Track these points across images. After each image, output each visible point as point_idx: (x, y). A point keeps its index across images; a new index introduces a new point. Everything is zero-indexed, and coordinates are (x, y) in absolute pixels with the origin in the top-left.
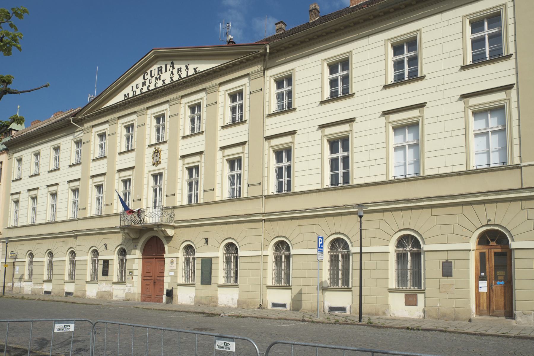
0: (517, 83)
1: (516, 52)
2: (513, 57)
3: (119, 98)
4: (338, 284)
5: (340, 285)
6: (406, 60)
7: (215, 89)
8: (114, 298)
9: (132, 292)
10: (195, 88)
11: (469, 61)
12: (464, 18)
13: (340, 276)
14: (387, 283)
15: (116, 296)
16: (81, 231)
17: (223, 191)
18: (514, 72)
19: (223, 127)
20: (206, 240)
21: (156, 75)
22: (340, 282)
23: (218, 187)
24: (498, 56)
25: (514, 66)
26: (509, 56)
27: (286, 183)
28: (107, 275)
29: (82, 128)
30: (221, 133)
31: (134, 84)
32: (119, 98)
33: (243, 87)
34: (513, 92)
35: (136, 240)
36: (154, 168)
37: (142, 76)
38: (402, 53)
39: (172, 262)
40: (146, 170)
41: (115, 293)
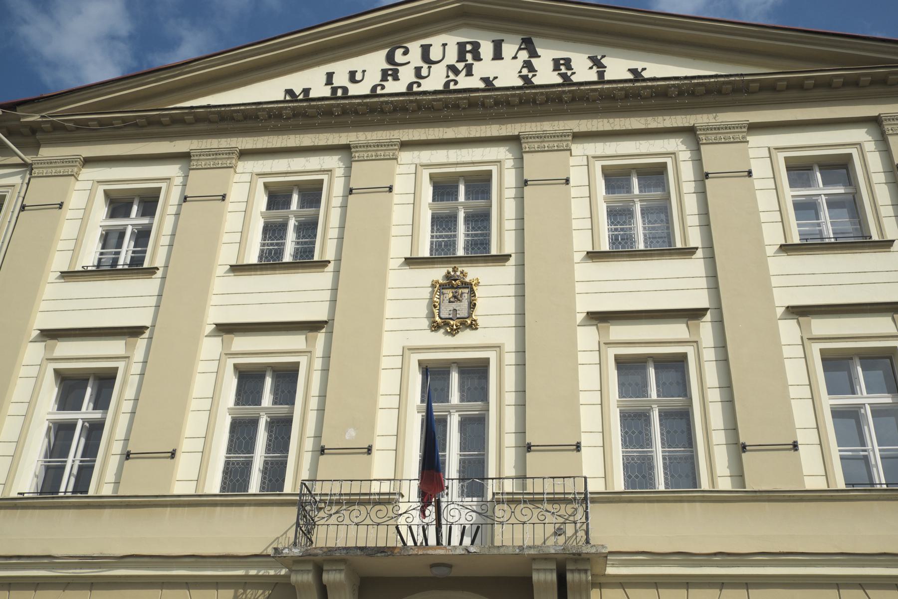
0: (153, 326)
1: (166, 267)
2: (331, 267)
3: (268, 91)
6: (292, 223)
7: (68, 169)
10: (336, 135)
11: (425, 252)
12: (419, 168)
16: (47, 560)
17: (199, 467)
18: (153, 301)
19: (68, 275)
21: (452, 57)
23: (188, 446)
24: (305, 260)
26: (324, 264)
27: (75, 471)
29: (28, 159)
30: (53, 290)
31: (355, 63)
32: (268, 91)
33: (164, 185)
34: (141, 343)
36: (440, 338)
37: (383, 53)
38: (127, 215)
40: (391, 345)
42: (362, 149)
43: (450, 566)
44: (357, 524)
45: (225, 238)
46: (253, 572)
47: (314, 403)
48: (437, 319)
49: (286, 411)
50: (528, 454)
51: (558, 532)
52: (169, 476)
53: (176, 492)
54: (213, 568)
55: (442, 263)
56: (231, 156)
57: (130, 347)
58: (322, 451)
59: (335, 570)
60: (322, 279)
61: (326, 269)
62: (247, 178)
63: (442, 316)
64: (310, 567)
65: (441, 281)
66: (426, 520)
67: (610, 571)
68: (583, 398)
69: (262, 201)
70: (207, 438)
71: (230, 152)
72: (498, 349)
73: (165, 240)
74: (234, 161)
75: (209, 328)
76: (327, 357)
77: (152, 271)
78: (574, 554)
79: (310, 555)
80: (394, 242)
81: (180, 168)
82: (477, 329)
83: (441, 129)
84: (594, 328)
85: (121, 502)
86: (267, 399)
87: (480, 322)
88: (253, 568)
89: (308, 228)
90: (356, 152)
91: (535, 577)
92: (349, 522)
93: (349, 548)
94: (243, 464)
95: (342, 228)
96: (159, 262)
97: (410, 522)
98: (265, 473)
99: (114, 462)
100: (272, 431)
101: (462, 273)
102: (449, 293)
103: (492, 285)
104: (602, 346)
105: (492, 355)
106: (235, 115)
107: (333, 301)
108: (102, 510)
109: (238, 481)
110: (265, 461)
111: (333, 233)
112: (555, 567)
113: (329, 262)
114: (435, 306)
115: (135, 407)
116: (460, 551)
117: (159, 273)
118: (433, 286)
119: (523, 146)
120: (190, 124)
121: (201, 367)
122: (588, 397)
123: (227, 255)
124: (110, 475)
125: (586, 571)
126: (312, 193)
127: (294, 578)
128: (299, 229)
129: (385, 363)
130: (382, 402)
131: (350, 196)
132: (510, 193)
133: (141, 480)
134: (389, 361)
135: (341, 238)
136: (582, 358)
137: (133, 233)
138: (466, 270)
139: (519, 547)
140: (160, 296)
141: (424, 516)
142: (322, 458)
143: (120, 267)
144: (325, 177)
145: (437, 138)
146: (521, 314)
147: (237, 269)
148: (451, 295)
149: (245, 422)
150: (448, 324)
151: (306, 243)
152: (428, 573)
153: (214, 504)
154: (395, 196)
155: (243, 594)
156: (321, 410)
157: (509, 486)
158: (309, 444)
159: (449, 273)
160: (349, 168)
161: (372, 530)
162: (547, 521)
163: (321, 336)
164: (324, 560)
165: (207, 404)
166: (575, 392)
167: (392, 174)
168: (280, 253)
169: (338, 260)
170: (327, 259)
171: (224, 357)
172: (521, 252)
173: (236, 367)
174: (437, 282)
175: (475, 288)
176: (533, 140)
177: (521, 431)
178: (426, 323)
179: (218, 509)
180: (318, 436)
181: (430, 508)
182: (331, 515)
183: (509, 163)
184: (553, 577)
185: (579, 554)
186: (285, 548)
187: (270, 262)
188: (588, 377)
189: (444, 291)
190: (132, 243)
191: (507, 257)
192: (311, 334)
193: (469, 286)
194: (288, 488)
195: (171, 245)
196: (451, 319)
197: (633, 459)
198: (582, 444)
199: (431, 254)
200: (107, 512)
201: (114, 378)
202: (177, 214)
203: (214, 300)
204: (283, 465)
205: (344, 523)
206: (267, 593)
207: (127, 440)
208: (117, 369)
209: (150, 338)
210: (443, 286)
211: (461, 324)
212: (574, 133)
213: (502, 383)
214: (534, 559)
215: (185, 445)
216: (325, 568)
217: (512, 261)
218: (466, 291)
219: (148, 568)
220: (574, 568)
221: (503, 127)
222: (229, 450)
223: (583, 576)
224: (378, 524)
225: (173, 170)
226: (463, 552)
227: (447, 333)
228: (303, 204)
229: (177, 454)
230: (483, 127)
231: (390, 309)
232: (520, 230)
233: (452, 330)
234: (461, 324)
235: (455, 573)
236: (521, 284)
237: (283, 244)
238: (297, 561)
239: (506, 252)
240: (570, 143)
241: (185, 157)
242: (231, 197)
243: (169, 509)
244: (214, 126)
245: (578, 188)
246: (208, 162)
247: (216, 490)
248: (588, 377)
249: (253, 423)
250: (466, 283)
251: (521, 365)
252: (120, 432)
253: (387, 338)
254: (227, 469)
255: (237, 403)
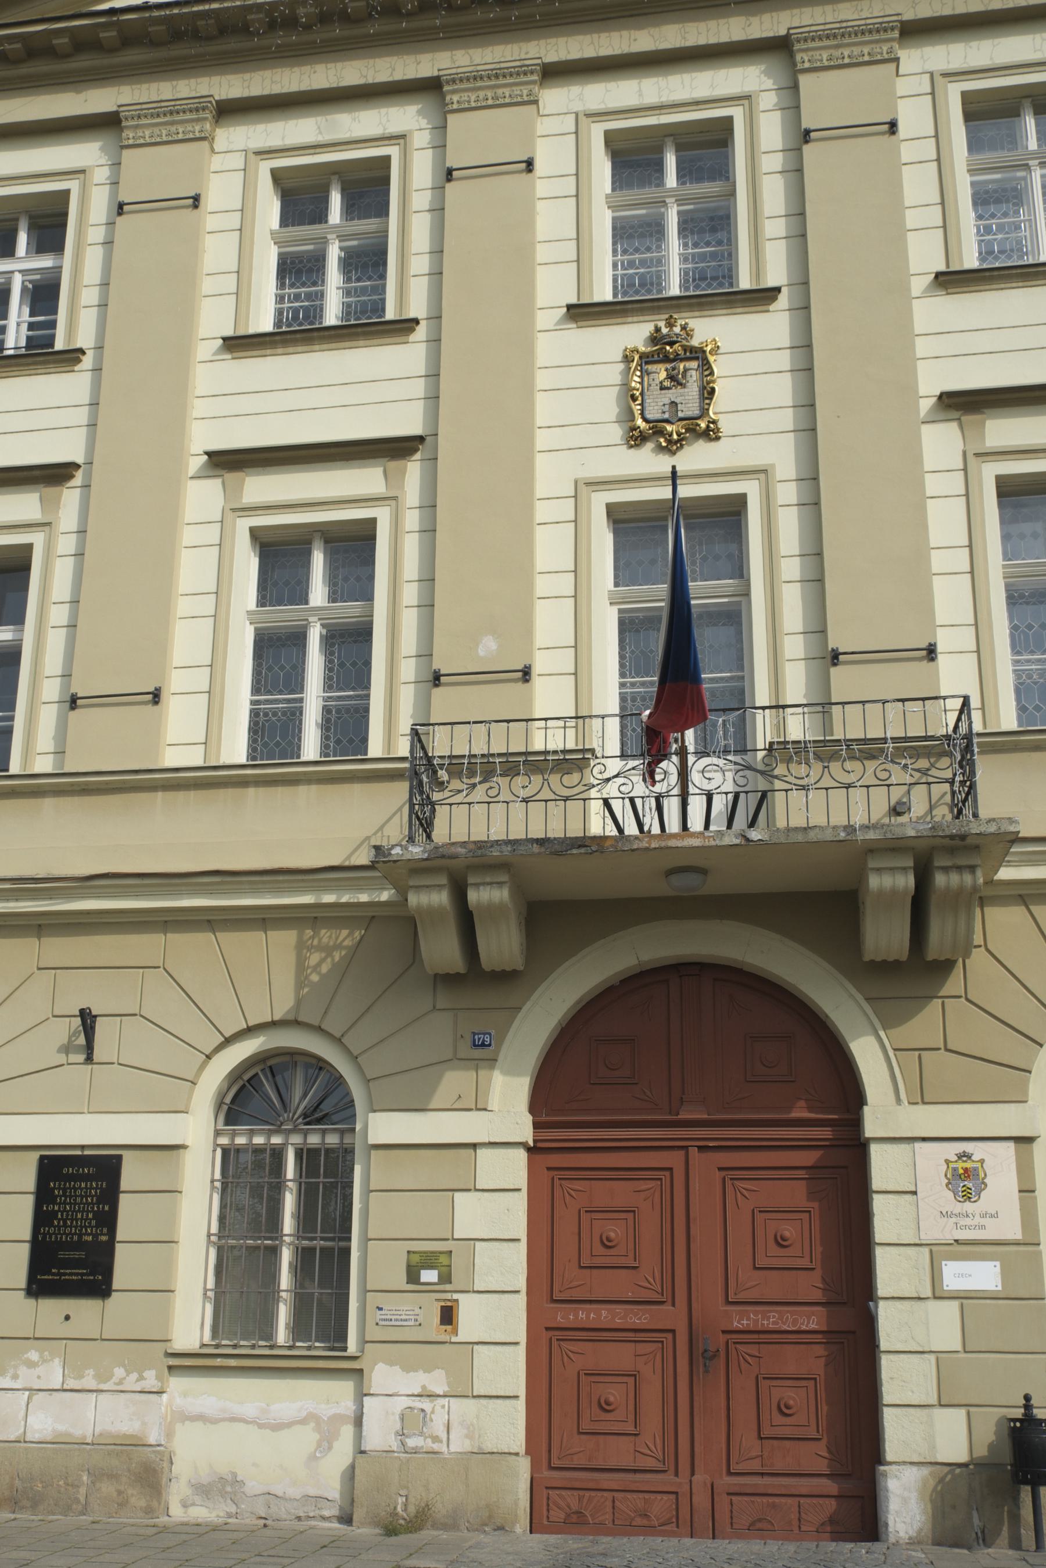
1: (99, 348)
2: (421, 332)
4: (267, 1331)
5: (282, 1336)
6: (334, 254)
8: (182, 1507)
9: (459, 1444)
10: (586, 39)
13: (285, 1280)
14: (165, 1315)
15: (222, 1486)
17: (206, 715)
18: (82, 416)
20: (88, 1020)
22: (283, 1314)
23: (183, 684)
24: (369, 325)
25: (84, 395)
26: (406, 326)
28: (95, 1281)
30: (213, 376)
33: (73, 185)
34: (70, 496)
35: (478, 987)
36: (649, 461)
39: (966, 1180)
40: (551, 477)
41: (193, 1455)
42: (465, 85)
43: (703, 871)
44: (526, 801)
45: (207, 285)
46: (329, 898)
47: (410, 594)
48: (640, 422)
49: (357, 612)
50: (834, 671)
51: (896, 811)
52: (155, 734)
53: (169, 763)
54: (255, 891)
55: (642, 311)
56: (201, 115)
57: (50, 505)
58: (437, 679)
59: (491, 884)
60: (407, 357)
61: (412, 337)
62: (237, 161)
63: (649, 416)
64: (443, 880)
65: (642, 349)
66: (658, 788)
67: (1005, 874)
68: (938, 561)
69: (269, 209)
70: (215, 667)
71: (197, 106)
72: (762, 476)
73: (90, 296)
74: (208, 126)
75: (197, 462)
76: (429, 506)
77: (72, 356)
78: (952, 837)
79: (443, 856)
80: (542, 276)
81: (101, 149)
82: (718, 438)
83: (625, 33)
84: (954, 425)
85: (72, 784)
86: (318, 593)
87: (725, 425)
88: (327, 889)
89: (368, 262)
90: (454, 92)
91: (874, 882)
92: (510, 797)
93: (516, 842)
94: (284, 714)
95: (438, 252)
96: (85, 339)
97: (615, 801)
98: (328, 729)
99: (48, 717)
100: (332, 653)
101: (684, 328)
102: (661, 372)
103: (746, 350)
104: (970, 458)
105: (751, 489)
106: (200, 23)
107: (433, 398)
108: (39, 800)
109: (278, 744)
110: (324, 707)
111: (420, 265)
112: (912, 865)
113: (416, 321)
114: (634, 398)
115: (74, 615)
116: (731, 839)
117: (87, 361)
118: (627, 359)
119: (798, 57)
120: (112, 50)
121: (189, 536)
122: (947, 560)
123: (216, 320)
124: (45, 739)
125: (972, 869)
126: (369, 187)
127: (414, 899)
128: (348, 264)
129: (542, 512)
130: (542, 585)
131: (449, 186)
132: (772, 162)
133: (105, 744)
134: (551, 511)
135: (437, 274)
136: (933, 485)
137: (24, 289)
138: (692, 323)
139: (845, 828)
140: (94, 404)
141: (654, 783)
142: (437, 692)
143: (11, 352)
144: (393, 151)
145: (618, 52)
146: (807, 405)
147: (238, 344)
148: (663, 375)
149: (279, 639)
150: (660, 432)
151: (363, 291)
152: (662, 888)
153: (243, 783)
154: (538, 182)
155: (313, 937)
156: (427, 606)
157: (797, 728)
158: (408, 670)
159: (658, 330)
160: (441, 128)
161: (556, 810)
162: (893, 780)
163: (413, 468)
164: (468, 867)
165: (207, 605)
166: (922, 551)
167: (530, 137)
168: (316, 311)
169: (436, 317)
170: (412, 315)
171: (230, 515)
172: (803, 283)
173: (254, 532)
174: (635, 350)
175: (711, 359)
176: (817, 44)
177: (818, 627)
178: (616, 433)
179: (251, 791)
180: (425, 654)
181: (664, 764)
182: (474, 785)
183: (768, 100)
184: (907, 882)
185: (963, 837)
186: (393, 847)
187: (299, 331)
188: (945, 522)
189: (650, 367)
190: (26, 310)
191: (771, 294)
192: (393, 465)
193: (698, 354)
194: (375, 748)
195: (103, 305)
196: (667, 421)
197: (1030, 677)
198: (940, 648)
199: (615, 295)
200: (48, 802)
201: (26, 568)
202: (108, 243)
203: (199, 408)
204: (362, 713)
205: (501, 798)
206: (357, 935)
207: (67, 676)
208: (29, 547)
209: (86, 486)
210: (646, 359)
211: (688, 430)
212: (902, 22)
213: (775, 539)
214: (871, 851)
215: (176, 682)
216: (471, 880)
217: (783, 300)
218: (694, 364)
219: (137, 896)
220: (949, 863)
221: (755, 20)
222: (256, 690)
223: (968, 878)
224: (566, 799)
225: (86, 153)
226: (737, 841)
227: (660, 449)
228: (350, 210)
229: (164, 695)
230: (712, 24)
231: (545, 409)
232: (799, 237)
233: (670, 442)
234: (688, 430)
235: (712, 886)
236: (804, 346)
237: (321, 295)
238: (419, 869)
239: (771, 282)
240: (896, 45)
241: (107, 123)
242: (211, 201)
243: (160, 794)
244: (163, 53)
245: (914, 146)
246: (156, 131)
247: (242, 758)
248: (945, 522)
249: (298, 638)
250: (692, 349)
251: (812, 504)
252: (53, 661)
253: (542, 463)
254: (256, 723)
255: (262, 601)
